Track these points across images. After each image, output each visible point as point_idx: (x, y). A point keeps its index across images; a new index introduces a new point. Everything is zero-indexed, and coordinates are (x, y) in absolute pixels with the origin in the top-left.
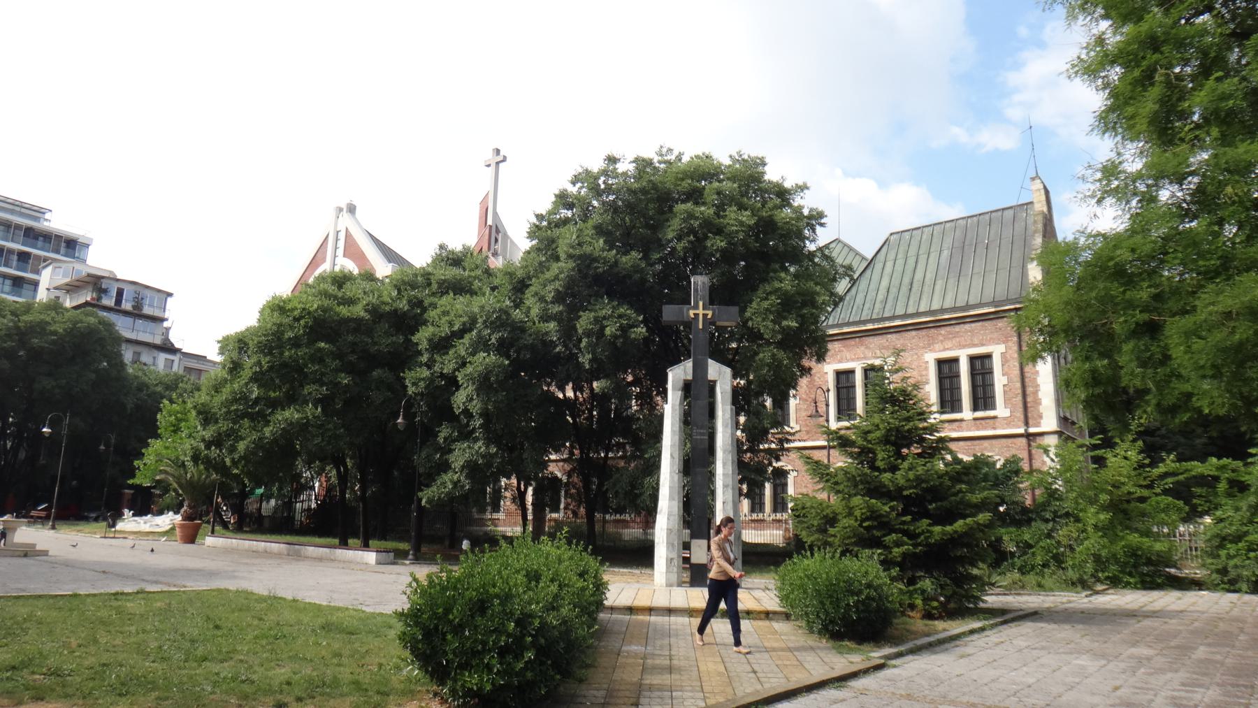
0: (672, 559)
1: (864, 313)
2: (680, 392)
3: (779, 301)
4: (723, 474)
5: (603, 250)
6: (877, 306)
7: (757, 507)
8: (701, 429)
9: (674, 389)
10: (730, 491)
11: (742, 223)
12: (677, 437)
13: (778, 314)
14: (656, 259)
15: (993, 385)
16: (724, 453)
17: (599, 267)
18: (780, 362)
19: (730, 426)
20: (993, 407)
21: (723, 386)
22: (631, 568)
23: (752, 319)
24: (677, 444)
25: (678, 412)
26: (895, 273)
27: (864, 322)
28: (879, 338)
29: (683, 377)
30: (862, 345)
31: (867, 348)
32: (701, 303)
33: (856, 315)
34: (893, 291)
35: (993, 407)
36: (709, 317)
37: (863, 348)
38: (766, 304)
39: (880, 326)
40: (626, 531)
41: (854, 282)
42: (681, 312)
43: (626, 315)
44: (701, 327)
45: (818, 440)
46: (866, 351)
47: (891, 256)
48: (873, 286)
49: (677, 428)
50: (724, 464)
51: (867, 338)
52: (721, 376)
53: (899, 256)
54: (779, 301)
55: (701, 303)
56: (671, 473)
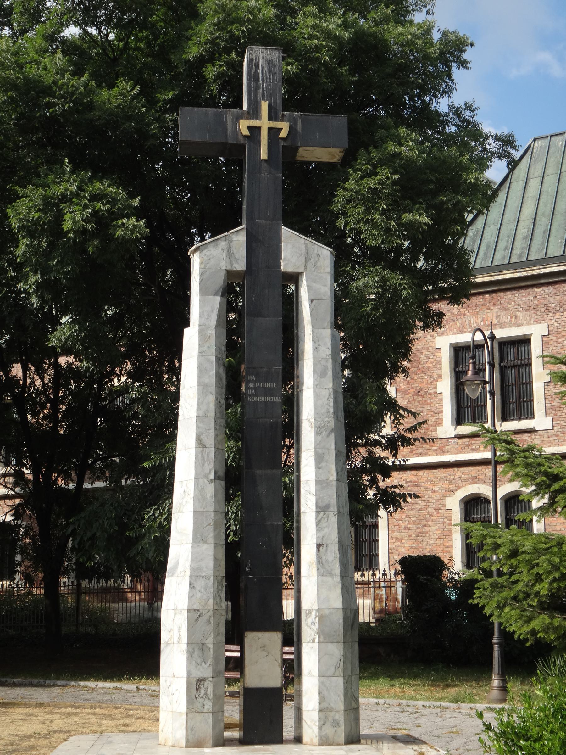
0: (200, 681)
1: (498, 256)
2: (218, 298)
3: (396, 177)
4: (317, 482)
5: (62, 72)
6: (518, 244)
7: (366, 561)
8: (266, 381)
9: (203, 291)
10: (334, 520)
11: (328, 35)
12: (211, 399)
13: (395, 202)
14: (166, 102)
15: (530, 383)
16: (318, 434)
17: (54, 105)
18: (396, 292)
19: (330, 373)
20: (530, 415)
21: (315, 286)
22: (120, 679)
23: (345, 214)
24: (212, 413)
25: (213, 342)
26: (543, 196)
27: (500, 268)
28: (523, 293)
29: (225, 265)
30: (495, 304)
31: (503, 309)
32: (264, 106)
33: (485, 258)
34: (543, 222)
35: (530, 415)
36: (283, 134)
37: (496, 310)
38: (372, 183)
39: (525, 274)
40: (120, 605)
41: (513, 165)
42: (221, 122)
43: (106, 196)
44: (264, 156)
45: (426, 454)
46: (503, 315)
47: (537, 171)
48: (510, 215)
49: (211, 378)
50: (319, 459)
51: (502, 294)
52: (310, 265)
53: (549, 171)
54: (396, 177)
55: (264, 106)
56: (196, 479)
